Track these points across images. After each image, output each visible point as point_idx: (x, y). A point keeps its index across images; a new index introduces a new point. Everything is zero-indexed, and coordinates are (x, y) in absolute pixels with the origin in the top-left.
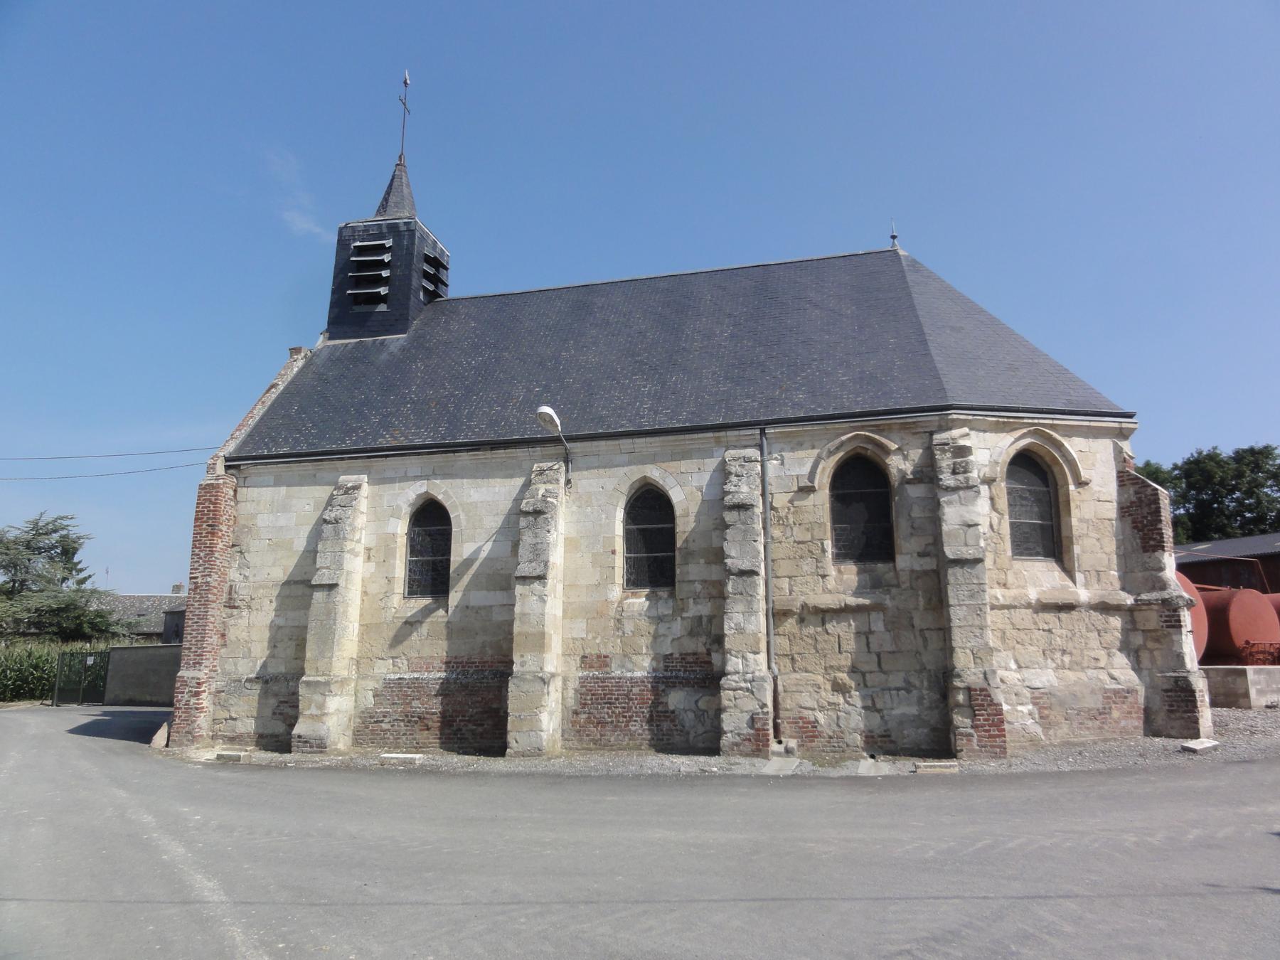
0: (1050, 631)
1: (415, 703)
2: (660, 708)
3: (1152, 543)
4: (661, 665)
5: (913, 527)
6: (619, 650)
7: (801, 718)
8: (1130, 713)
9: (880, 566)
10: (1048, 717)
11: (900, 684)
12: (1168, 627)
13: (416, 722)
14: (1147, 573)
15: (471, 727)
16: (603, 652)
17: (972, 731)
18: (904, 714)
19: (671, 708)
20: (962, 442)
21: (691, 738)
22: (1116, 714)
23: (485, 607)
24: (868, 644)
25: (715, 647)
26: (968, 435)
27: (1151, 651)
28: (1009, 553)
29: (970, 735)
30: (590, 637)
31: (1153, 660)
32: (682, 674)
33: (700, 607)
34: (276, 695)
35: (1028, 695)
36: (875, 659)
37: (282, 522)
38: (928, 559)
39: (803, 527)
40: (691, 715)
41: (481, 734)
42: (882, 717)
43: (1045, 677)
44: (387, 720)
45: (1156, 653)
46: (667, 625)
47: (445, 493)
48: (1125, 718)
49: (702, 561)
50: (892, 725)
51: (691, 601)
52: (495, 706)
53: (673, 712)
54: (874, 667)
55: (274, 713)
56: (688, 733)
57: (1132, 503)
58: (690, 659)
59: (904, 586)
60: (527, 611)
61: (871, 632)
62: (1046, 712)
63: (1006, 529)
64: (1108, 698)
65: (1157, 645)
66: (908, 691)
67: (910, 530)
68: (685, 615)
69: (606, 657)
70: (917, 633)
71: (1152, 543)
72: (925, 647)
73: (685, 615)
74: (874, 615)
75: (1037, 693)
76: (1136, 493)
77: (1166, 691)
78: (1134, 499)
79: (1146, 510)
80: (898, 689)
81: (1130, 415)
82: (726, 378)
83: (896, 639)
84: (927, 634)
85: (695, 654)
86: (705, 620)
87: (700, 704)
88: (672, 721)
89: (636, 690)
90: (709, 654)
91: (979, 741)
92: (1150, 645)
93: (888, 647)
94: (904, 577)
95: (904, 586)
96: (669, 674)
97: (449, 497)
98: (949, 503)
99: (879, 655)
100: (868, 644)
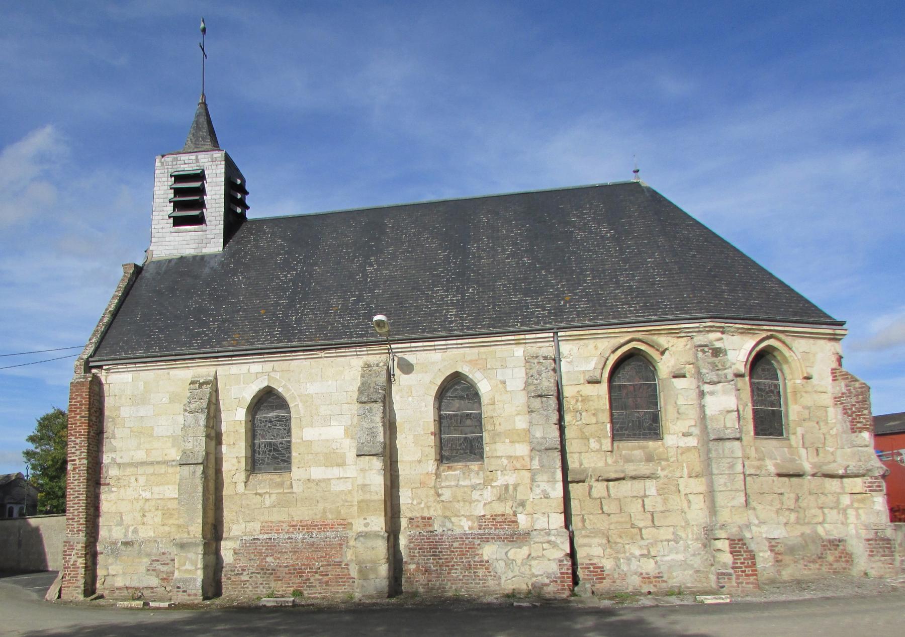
0: (782, 494)
1: (269, 559)
2: (477, 559)
3: (859, 425)
4: (476, 524)
5: (678, 412)
6: (440, 512)
7: (591, 564)
8: (840, 557)
9: (651, 444)
10: (781, 561)
11: (671, 537)
12: (871, 491)
13: (272, 574)
14: (856, 449)
15: (317, 576)
16: (426, 515)
17: (732, 571)
18: (673, 560)
19: (485, 558)
20: (718, 345)
21: (503, 581)
22: (830, 558)
23: (324, 480)
24: (643, 506)
25: (520, 509)
26: (721, 339)
27: (857, 509)
28: (752, 433)
29: (730, 574)
30: (415, 502)
31: (858, 516)
32: (492, 531)
33: (506, 477)
34: (148, 555)
35: (767, 544)
36: (650, 516)
37: (142, 412)
38: (690, 438)
39: (589, 413)
40: (502, 563)
41: (327, 582)
42: (656, 562)
43: (779, 533)
44: (245, 573)
45: (861, 511)
46: (480, 492)
47: (284, 387)
48: (837, 561)
49: (507, 441)
50: (664, 568)
51: (499, 473)
52: (337, 560)
53: (487, 562)
54: (649, 523)
55: (148, 570)
56: (500, 578)
57: (843, 394)
58: (499, 519)
59: (672, 460)
60: (368, 482)
61: (645, 496)
62: (780, 557)
63: (749, 414)
64: (824, 546)
65: (862, 505)
66: (677, 543)
67: (676, 415)
68: (494, 484)
69: (430, 518)
70: (683, 497)
71: (859, 425)
72: (689, 507)
73: (494, 484)
74: (648, 482)
75: (773, 543)
76: (847, 386)
77: (868, 540)
78: (844, 390)
79: (854, 400)
80: (668, 541)
81: (841, 324)
82: (515, 291)
83: (665, 501)
84: (691, 497)
85: (503, 515)
86: (511, 488)
87: (509, 554)
88: (487, 569)
89: (456, 544)
90: (515, 515)
91: (737, 579)
92: (856, 505)
93: (660, 508)
94: (672, 452)
95: (672, 460)
96: (481, 531)
97: (288, 390)
98: (712, 393)
99: (652, 515)
100: (643, 506)
